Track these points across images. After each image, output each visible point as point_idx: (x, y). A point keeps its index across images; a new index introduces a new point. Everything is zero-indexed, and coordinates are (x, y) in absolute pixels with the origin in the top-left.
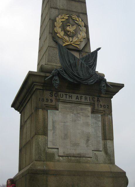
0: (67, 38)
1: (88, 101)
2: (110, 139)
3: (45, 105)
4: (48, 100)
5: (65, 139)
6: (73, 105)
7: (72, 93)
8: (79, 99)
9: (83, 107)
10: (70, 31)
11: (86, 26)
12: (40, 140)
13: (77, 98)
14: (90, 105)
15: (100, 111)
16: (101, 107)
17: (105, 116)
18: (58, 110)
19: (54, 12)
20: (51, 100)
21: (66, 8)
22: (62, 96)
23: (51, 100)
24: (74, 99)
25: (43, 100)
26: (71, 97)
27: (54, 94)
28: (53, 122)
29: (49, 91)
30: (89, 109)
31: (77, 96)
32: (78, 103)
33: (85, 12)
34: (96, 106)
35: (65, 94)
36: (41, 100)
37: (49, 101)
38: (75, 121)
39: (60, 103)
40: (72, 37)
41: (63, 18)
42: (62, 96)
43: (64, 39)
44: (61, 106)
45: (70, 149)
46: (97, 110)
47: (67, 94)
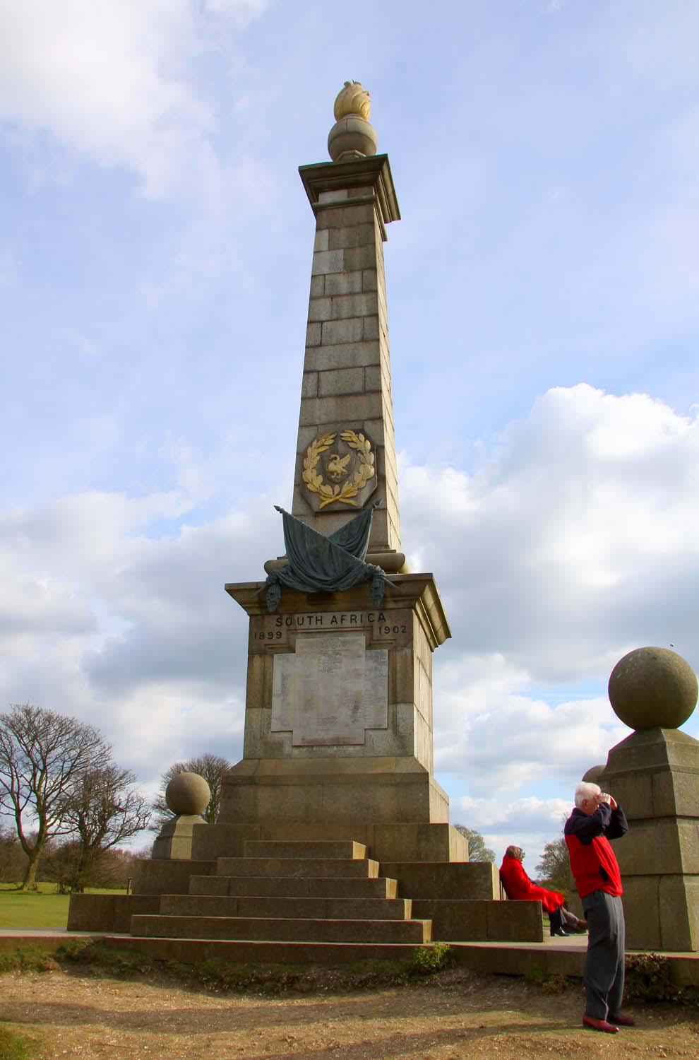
0: (327, 489)
1: (359, 624)
2: (404, 702)
3: (268, 646)
4: (272, 635)
6: (327, 637)
7: (321, 612)
9: (349, 637)
10: (336, 471)
11: (378, 450)
13: (334, 620)
15: (384, 642)
18: (295, 652)
19: (312, 432)
24: (327, 623)
25: (262, 636)
26: (321, 620)
27: (284, 621)
28: (284, 678)
30: (362, 639)
31: (334, 617)
34: (376, 632)
36: (258, 636)
37: (275, 636)
38: (329, 670)
40: (341, 483)
41: (323, 445)
43: (321, 492)
44: (300, 642)
46: (378, 640)
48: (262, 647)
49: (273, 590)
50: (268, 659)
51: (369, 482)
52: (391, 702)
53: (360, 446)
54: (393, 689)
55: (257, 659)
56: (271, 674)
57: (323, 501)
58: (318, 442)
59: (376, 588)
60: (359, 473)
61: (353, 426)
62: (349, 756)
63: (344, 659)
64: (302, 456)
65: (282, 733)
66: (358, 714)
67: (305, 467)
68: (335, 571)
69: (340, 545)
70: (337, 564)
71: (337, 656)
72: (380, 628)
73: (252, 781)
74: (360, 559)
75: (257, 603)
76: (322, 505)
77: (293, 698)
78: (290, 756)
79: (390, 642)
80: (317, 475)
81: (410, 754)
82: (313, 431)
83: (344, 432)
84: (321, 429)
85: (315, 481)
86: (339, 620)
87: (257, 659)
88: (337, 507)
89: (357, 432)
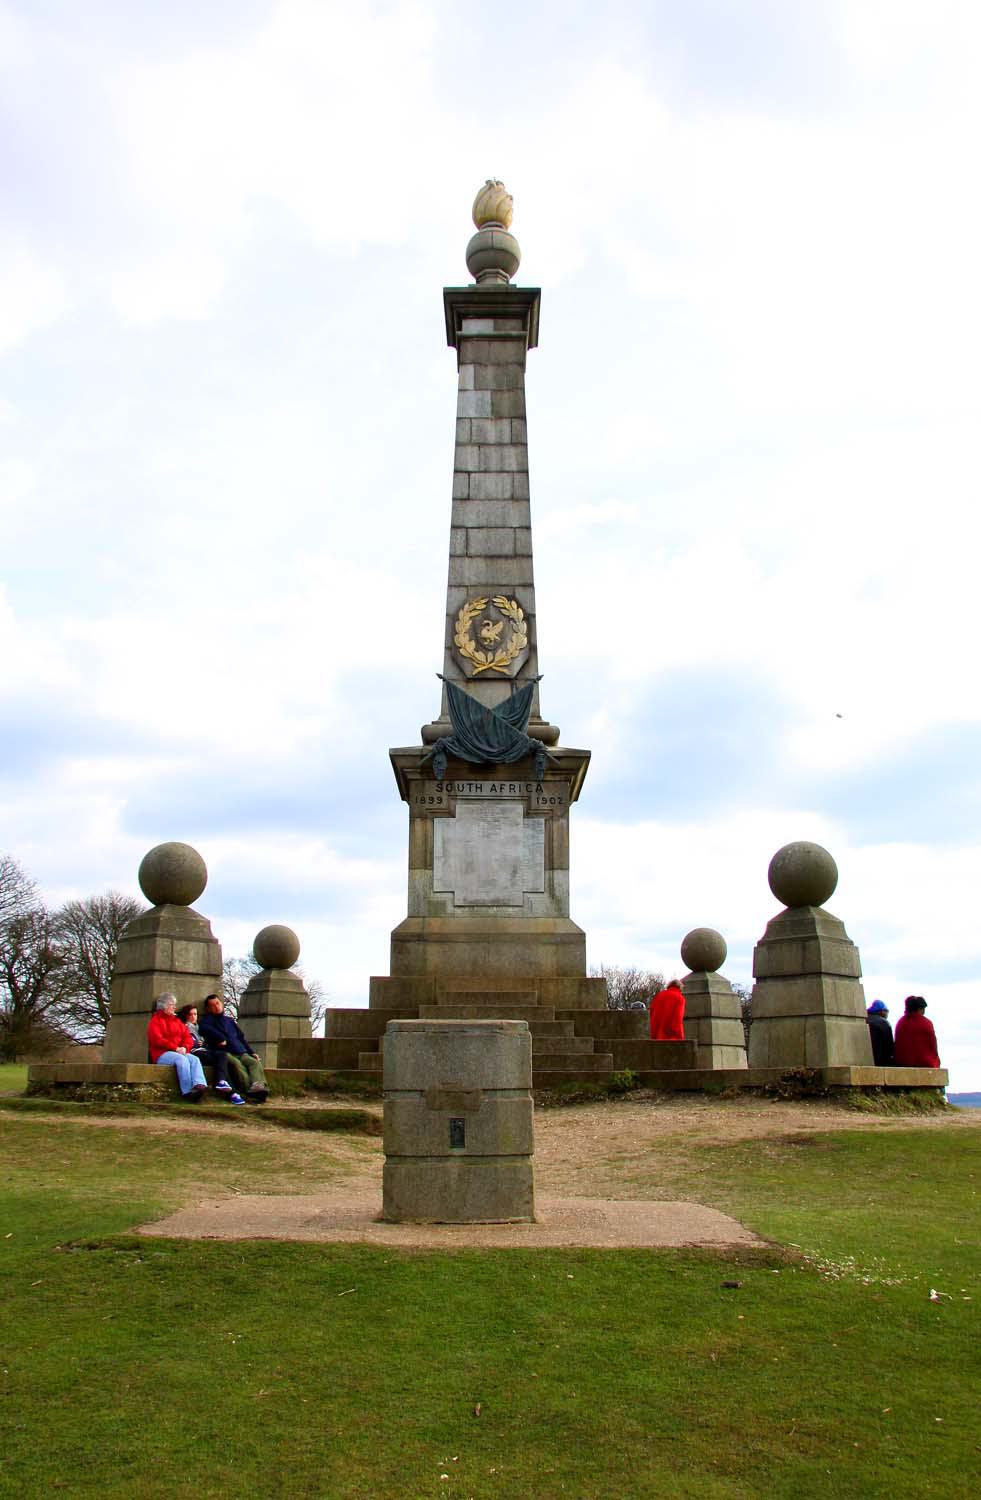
0: (480, 656)
1: (518, 794)
5: (467, 872)
9: (508, 805)
11: (530, 618)
13: (493, 788)
18: (454, 817)
19: (461, 594)
21: (483, 581)
30: (520, 808)
38: (488, 836)
39: (459, 802)
40: (494, 651)
44: (460, 808)
50: (429, 823)
51: (523, 651)
52: (548, 867)
53: (513, 614)
59: (540, 763)
61: (505, 591)
64: (452, 619)
73: (421, 938)
76: (476, 671)
78: (453, 915)
80: (470, 640)
85: (468, 647)
88: (490, 675)
89: (511, 598)
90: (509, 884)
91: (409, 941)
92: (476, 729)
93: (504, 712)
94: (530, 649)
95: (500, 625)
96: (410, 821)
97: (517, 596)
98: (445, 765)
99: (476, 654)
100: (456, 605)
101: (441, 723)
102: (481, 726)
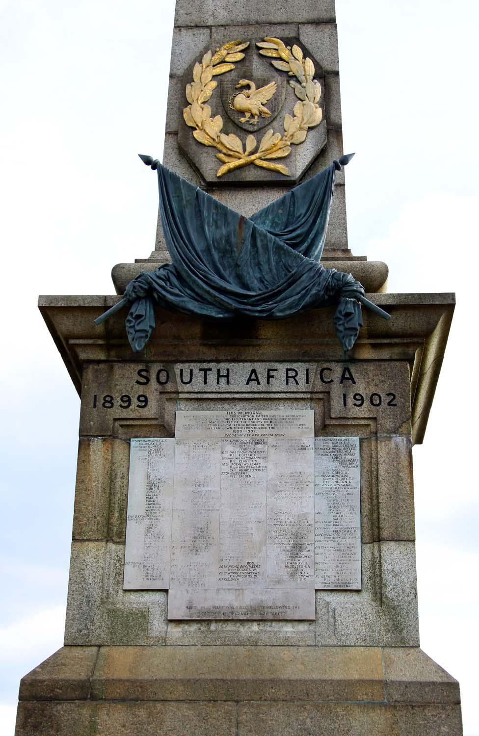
0: (232, 141)
1: (302, 386)
2: (397, 539)
4: (129, 401)
5: (195, 550)
6: (238, 407)
8: (259, 383)
9: (283, 411)
10: (249, 111)
11: (328, 77)
12: (88, 559)
13: (253, 376)
14: (311, 399)
16: (359, 403)
17: (377, 439)
18: (173, 436)
19: (196, 40)
20: (142, 399)
21: (241, 18)
22: (186, 379)
23: (142, 399)
25: (109, 402)
26: (227, 376)
27: (153, 377)
29: (132, 366)
30: (308, 416)
31: (254, 371)
32: (289, 399)
33: (325, 15)
35: (201, 370)
37: (135, 402)
38: (243, 473)
39: (183, 405)
40: (259, 132)
41: (223, 62)
42: (186, 379)
43: (219, 146)
44: (184, 417)
45: (218, 590)
47: (212, 365)
48: (103, 428)
49: (140, 309)
50: (119, 446)
51: (312, 133)
52: (367, 539)
53: (295, 67)
54: (371, 512)
55: (97, 445)
56: (126, 476)
57: (224, 163)
58: (213, 55)
59: (348, 315)
60: (294, 116)
61: (279, 30)
62: (286, 644)
63: (272, 451)
64: (181, 80)
65: (145, 595)
66: (302, 559)
67: (190, 101)
68: (261, 281)
69: (271, 233)
70: (265, 267)
71: (259, 446)
72: (345, 396)
73: (87, 692)
74: (312, 260)
75: (99, 337)
76: (223, 169)
77: (170, 526)
78: (163, 641)
79: (363, 422)
80: (213, 116)
81: (411, 643)
82: (202, 37)
83: (264, 41)
84: (218, 35)
85: (209, 126)
86: (263, 379)
87: (97, 445)
88: (251, 175)
89: (289, 42)
90: (284, 573)
91: (56, 699)
92: (216, 256)
93: (274, 224)
94: (328, 131)
95: (269, 91)
96: (80, 443)
97: (302, 38)
98: (149, 323)
99: (223, 137)
100: (188, 58)
101: (153, 261)
102: (227, 251)
